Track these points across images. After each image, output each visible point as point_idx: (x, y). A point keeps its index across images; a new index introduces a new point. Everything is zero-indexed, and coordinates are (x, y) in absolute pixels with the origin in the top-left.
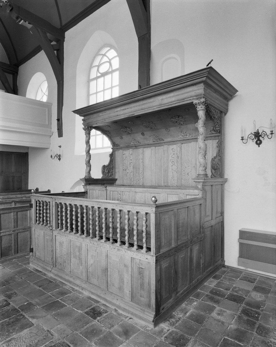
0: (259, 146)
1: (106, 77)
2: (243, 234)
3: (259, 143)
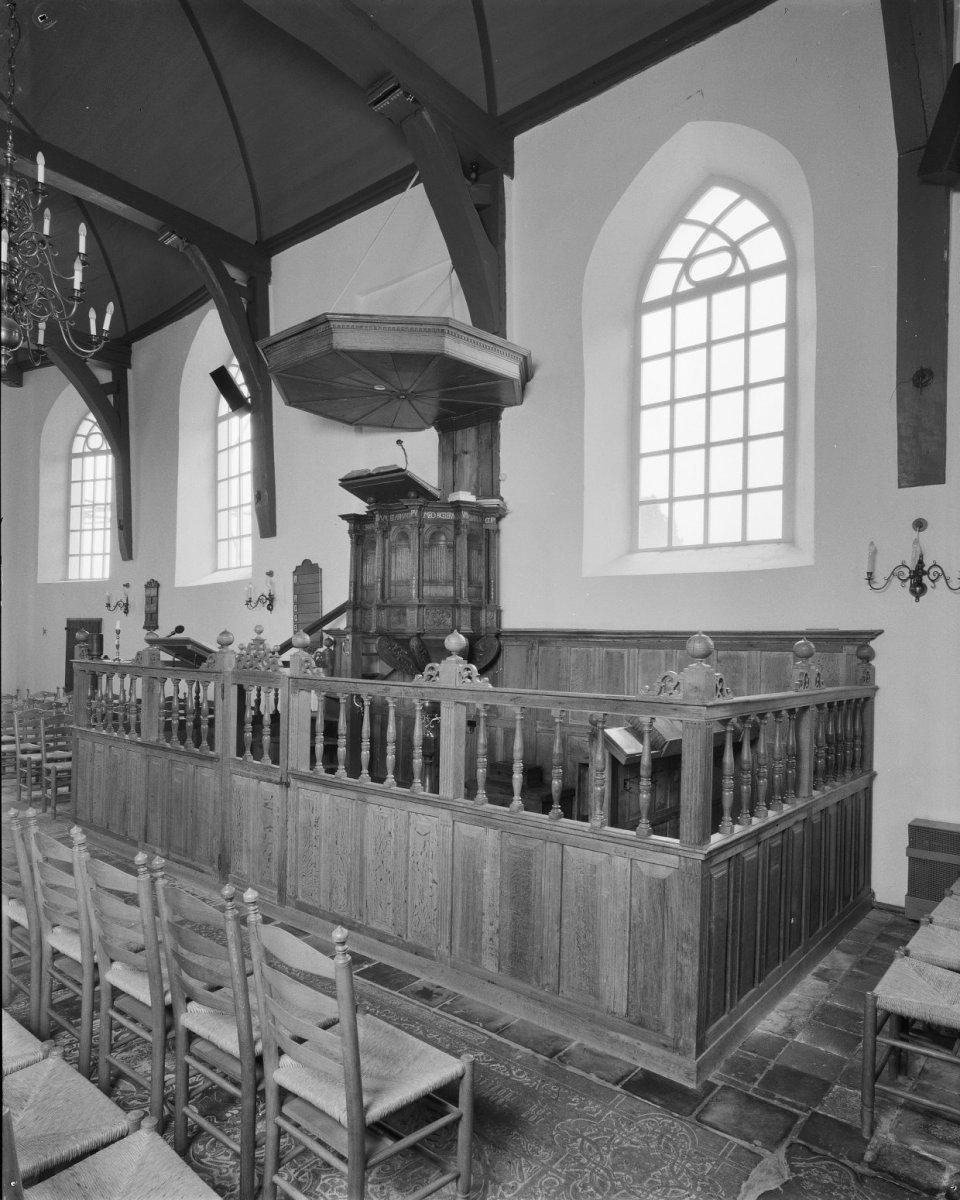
0: (917, 599)
1: (719, 298)
2: (922, 835)
3: (918, 588)
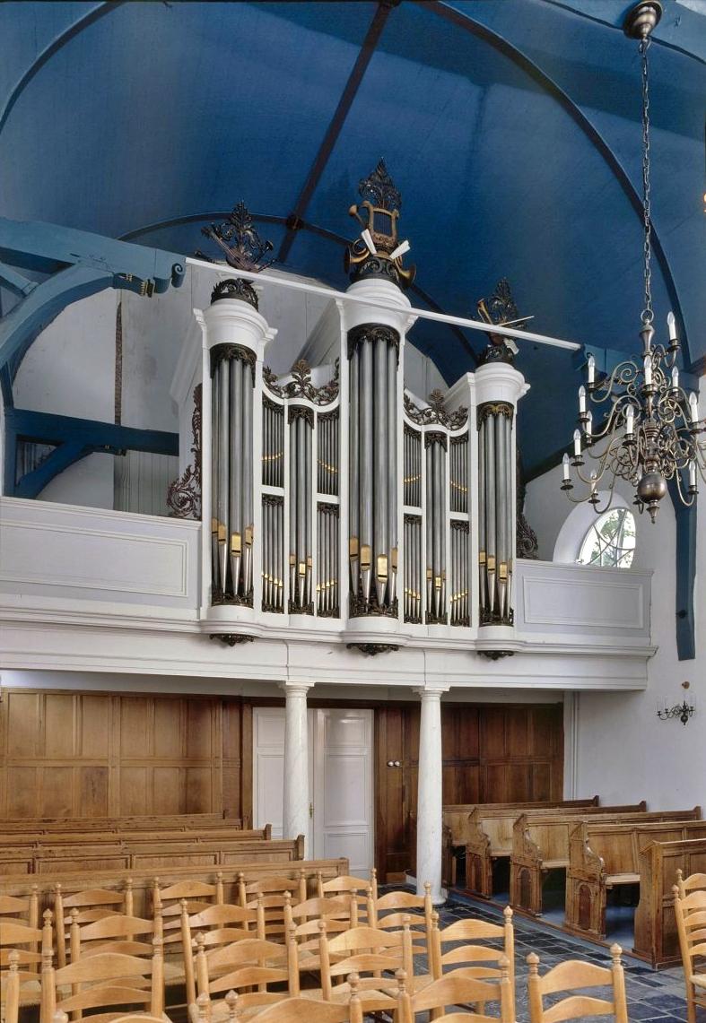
3: (684, 720)
